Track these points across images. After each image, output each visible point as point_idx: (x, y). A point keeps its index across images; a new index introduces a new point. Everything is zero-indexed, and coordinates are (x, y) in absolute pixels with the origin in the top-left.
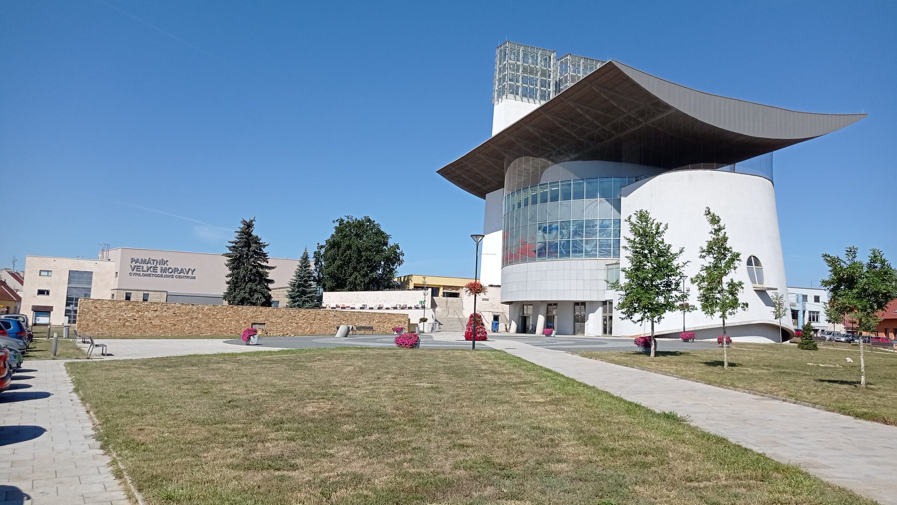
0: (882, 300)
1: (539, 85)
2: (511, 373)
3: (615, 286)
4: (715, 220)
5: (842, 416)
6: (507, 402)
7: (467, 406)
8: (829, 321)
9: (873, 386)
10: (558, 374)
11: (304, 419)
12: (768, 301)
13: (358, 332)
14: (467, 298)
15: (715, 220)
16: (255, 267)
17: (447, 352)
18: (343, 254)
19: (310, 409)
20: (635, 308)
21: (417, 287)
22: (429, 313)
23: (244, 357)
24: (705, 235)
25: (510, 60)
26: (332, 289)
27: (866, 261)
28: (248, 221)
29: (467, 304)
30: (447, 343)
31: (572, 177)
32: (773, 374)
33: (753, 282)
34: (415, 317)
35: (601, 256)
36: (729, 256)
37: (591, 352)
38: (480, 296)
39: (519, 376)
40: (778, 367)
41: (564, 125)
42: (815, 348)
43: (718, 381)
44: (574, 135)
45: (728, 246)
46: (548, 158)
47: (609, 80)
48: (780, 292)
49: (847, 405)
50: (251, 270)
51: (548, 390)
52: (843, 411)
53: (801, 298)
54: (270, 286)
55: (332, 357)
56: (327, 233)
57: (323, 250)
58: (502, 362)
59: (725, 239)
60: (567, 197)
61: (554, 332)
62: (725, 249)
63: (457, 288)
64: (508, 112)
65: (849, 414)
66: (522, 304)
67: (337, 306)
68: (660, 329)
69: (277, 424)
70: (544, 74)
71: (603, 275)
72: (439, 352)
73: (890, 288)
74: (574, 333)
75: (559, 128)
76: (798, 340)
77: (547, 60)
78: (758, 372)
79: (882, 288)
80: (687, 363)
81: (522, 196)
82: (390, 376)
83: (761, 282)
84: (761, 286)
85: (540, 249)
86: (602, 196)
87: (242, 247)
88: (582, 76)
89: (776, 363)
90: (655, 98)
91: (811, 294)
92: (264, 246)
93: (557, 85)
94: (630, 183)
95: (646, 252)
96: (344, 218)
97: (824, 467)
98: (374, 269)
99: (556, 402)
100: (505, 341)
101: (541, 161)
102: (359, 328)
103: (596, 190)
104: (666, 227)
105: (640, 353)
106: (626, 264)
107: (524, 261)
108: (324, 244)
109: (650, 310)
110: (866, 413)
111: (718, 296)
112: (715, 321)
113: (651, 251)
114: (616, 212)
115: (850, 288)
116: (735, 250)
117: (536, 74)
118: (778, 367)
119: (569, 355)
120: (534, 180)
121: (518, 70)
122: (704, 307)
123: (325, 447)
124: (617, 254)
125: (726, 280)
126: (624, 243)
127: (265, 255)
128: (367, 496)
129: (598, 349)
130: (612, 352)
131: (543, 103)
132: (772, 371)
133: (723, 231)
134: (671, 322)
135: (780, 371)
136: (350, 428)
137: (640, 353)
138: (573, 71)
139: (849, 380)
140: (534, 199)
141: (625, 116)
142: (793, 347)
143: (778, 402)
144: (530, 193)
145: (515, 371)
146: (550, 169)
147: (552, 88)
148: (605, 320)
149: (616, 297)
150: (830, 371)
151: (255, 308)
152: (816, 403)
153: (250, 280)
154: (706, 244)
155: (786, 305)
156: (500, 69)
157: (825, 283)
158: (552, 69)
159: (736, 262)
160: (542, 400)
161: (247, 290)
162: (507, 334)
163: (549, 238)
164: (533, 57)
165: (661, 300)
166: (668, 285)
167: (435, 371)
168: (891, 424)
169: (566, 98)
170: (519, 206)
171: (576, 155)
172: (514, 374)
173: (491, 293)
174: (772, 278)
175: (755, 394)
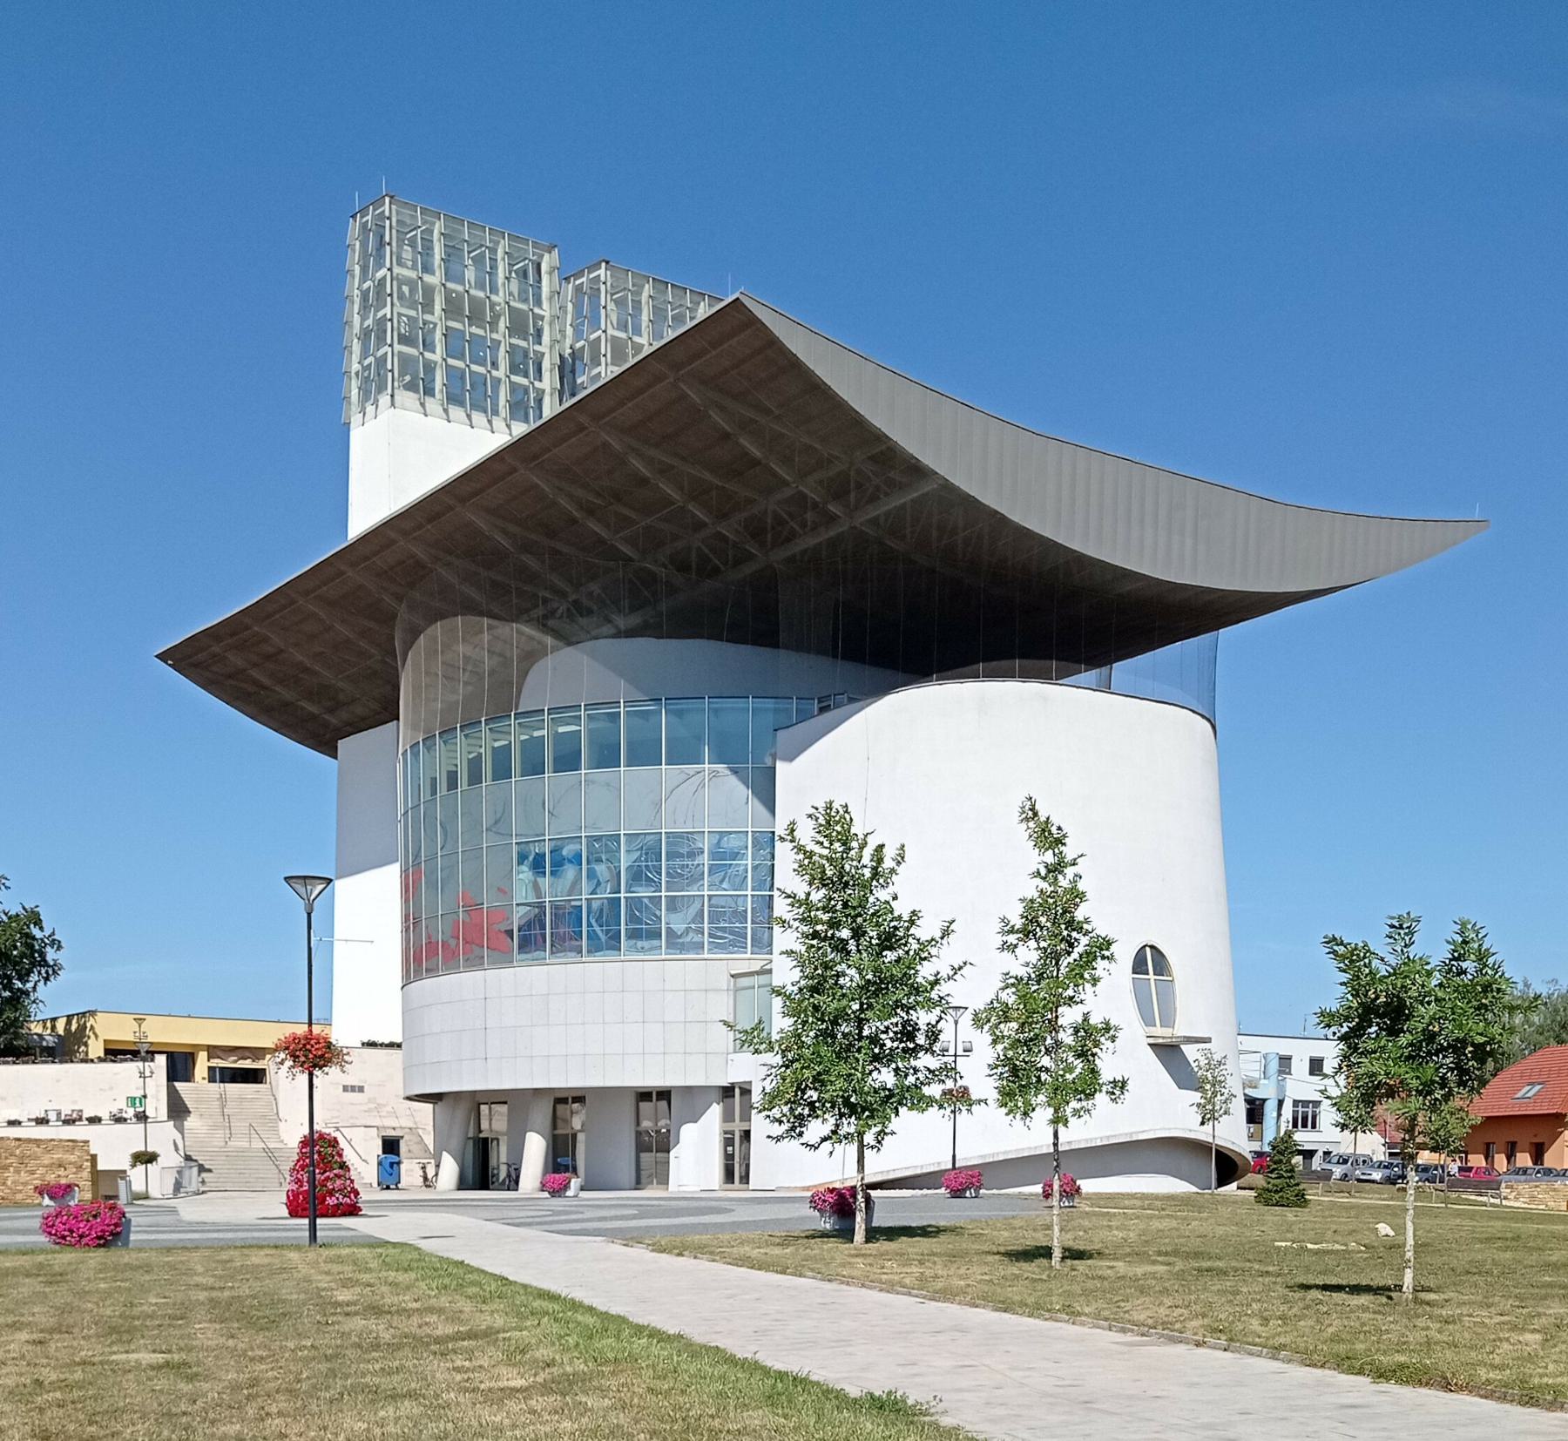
0: (1476, 1061)
1: (503, 364)
2: (431, 1310)
3: (752, 1038)
4: (1048, 837)
5: (1343, 1376)
6: (412, 1395)
7: (280, 1414)
8: (1344, 1127)
9: (1432, 1296)
10: (575, 1306)
12: (1184, 1076)
14: (286, 1082)
15: (1048, 837)
17: (224, 1256)
20: (811, 1105)
21: (114, 1053)
22: (162, 1136)
24: (1017, 879)
25: (397, 265)
29: (288, 1106)
30: (216, 1227)
31: (622, 690)
32: (1180, 1275)
33: (1148, 1021)
35: (715, 947)
37: (680, 1240)
38: (327, 1080)
39: (455, 1317)
40: (1197, 1255)
41: (590, 511)
42: (1301, 1201)
43: (1030, 1300)
44: (626, 549)
45: (1079, 915)
46: (543, 624)
47: (731, 363)
48: (1217, 1049)
49: (1360, 1347)
51: (543, 1353)
52: (1347, 1363)
53: (1274, 1065)
58: (402, 1277)
59: (1077, 896)
60: (607, 757)
61: (575, 1183)
62: (1072, 925)
63: (257, 1053)
64: (403, 455)
65: (1360, 1372)
66: (475, 1102)
68: (880, 1165)
70: (519, 325)
71: (722, 1007)
72: (196, 1255)
73: (1496, 1030)
74: (638, 1184)
75: (574, 521)
76: (1258, 1180)
77: (528, 277)
78: (1140, 1271)
79: (1476, 1030)
80: (952, 1257)
81: (461, 750)
82: (24, 1336)
83: (1168, 1021)
84: (1167, 1032)
85: (526, 927)
86: (718, 758)
88: (647, 343)
89: (1195, 1243)
90: (880, 437)
91: (1301, 1053)
93: (567, 370)
94: (803, 717)
95: (845, 933)
99: (565, 1385)
100: (427, 1216)
101: (519, 633)
103: (699, 739)
104: (900, 858)
105: (824, 1235)
106: (787, 975)
107: (475, 963)
109: (853, 1110)
110: (1402, 1366)
111: (1046, 1061)
112: (1031, 1135)
113: (858, 933)
114: (762, 810)
115: (1393, 1032)
116: (1101, 928)
117: (493, 325)
118: (1197, 1255)
119: (617, 1248)
120: (500, 699)
121: (428, 307)
122: (1006, 1096)
124: (763, 944)
125: (1069, 1016)
126: (781, 908)
129: (706, 1228)
130: (744, 1235)
131: (520, 429)
132: (1180, 1265)
133: (1070, 872)
134: (915, 1142)
135: (1198, 1265)
137: (824, 1235)
138: (619, 324)
139: (1374, 1284)
141: (788, 492)
142: (1244, 1201)
143: (1181, 1348)
144: (487, 742)
145: (444, 1301)
146: (549, 662)
148: (728, 1142)
149: (755, 1071)
150: (1330, 1261)
152: (1282, 1347)
154: (1020, 908)
155: (1234, 1085)
156: (365, 295)
157: (1328, 1019)
158: (546, 310)
159: (1100, 964)
160: (519, 1383)
163: (552, 890)
164: (478, 261)
165: (885, 1077)
166: (908, 1032)
167: (182, 1313)
168: (1460, 1389)
169: (405, 533)
170: (452, 782)
171: (634, 620)
172: (440, 1311)
173: (363, 1067)
174: (1200, 1008)
175: (1123, 1330)
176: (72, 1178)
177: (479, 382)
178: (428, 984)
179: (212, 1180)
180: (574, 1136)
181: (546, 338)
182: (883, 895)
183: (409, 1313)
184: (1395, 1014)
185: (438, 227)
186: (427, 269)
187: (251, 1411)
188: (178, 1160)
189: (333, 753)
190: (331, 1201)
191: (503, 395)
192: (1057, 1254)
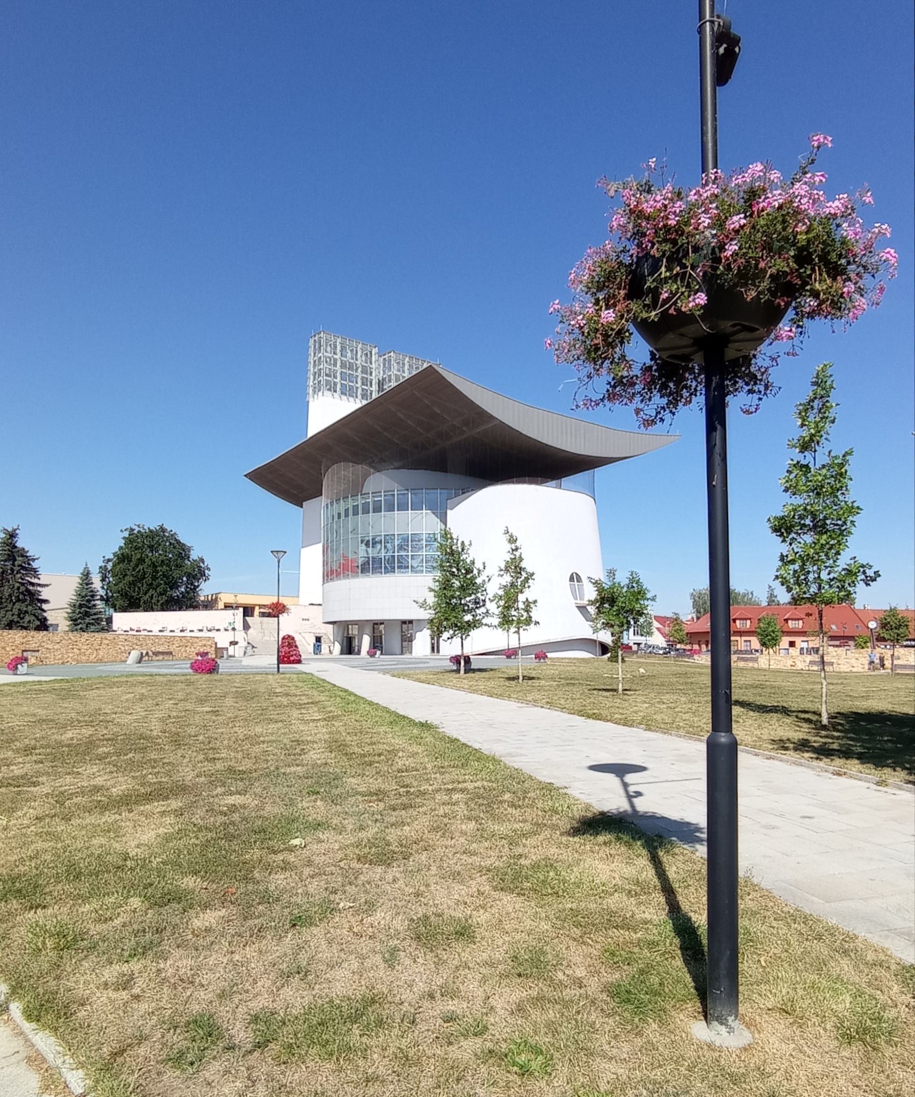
3: (423, 605)
4: (512, 540)
11: (60, 744)
13: (154, 658)
15: (512, 540)
16: (23, 584)
18: (134, 570)
19: (70, 735)
21: (227, 607)
22: (240, 636)
23: (6, 688)
24: (502, 555)
25: (325, 351)
26: (124, 610)
27: (624, 582)
28: (10, 530)
34: (223, 640)
36: (524, 575)
46: (370, 465)
50: (18, 588)
54: (45, 606)
55: (118, 684)
56: (113, 544)
57: (111, 564)
59: (521, 559)
60: (390, 508)
64: (326, 411)
67: (132, 630)
69: (28, 750)
74: (402, 653)
77: (368, 356)
84: (582, 602)
87: (5, 561)
88: (407, 375)
92: (34, 560)
93: (381, 384)
94: (456, 495)
96: (134, 527)
97: (521, 755)
98: (174, 585)
102: (156, 654)
104: (470, 545)
105: (453, 671)
107: (347, 577)
108: (112, 557)
109: (460, 628)
111: (514, 613)
116: (530, 570)
119: (381, 675)
120: (356, 489)
121: (335, 365)
123: (73, 767)
125: (521, 598)
127: (35, 570)
128: (100, 801)
131: (365, 402)
136: (106, 750)
140: (356, 508)
144: (350, 503)
147: (375, 388)
151: (25, 633)
153: (18, 600)
154: (504, 564)
158: (373, 366)
159: (530, 581)
161: (16, 611)
162: (330, 656)
163: (372, 552)
165: (468, 617)
168: (608, 721)
171: (400, 464)
176: (209, 650)
177: (351, 388)
178: (331, 584)
179: (250, 650)
180: (381, 637)
181: (374, 374)
182: (464, 556)
183: (296, 696)
184: (612, 601)
185: (339, 340)
186: (335, 353)
187: (230, 725)
188: (246, 644)
189: (302, 507)
190: (292, 659)
191: (360, 391)
192: (521, 678)
